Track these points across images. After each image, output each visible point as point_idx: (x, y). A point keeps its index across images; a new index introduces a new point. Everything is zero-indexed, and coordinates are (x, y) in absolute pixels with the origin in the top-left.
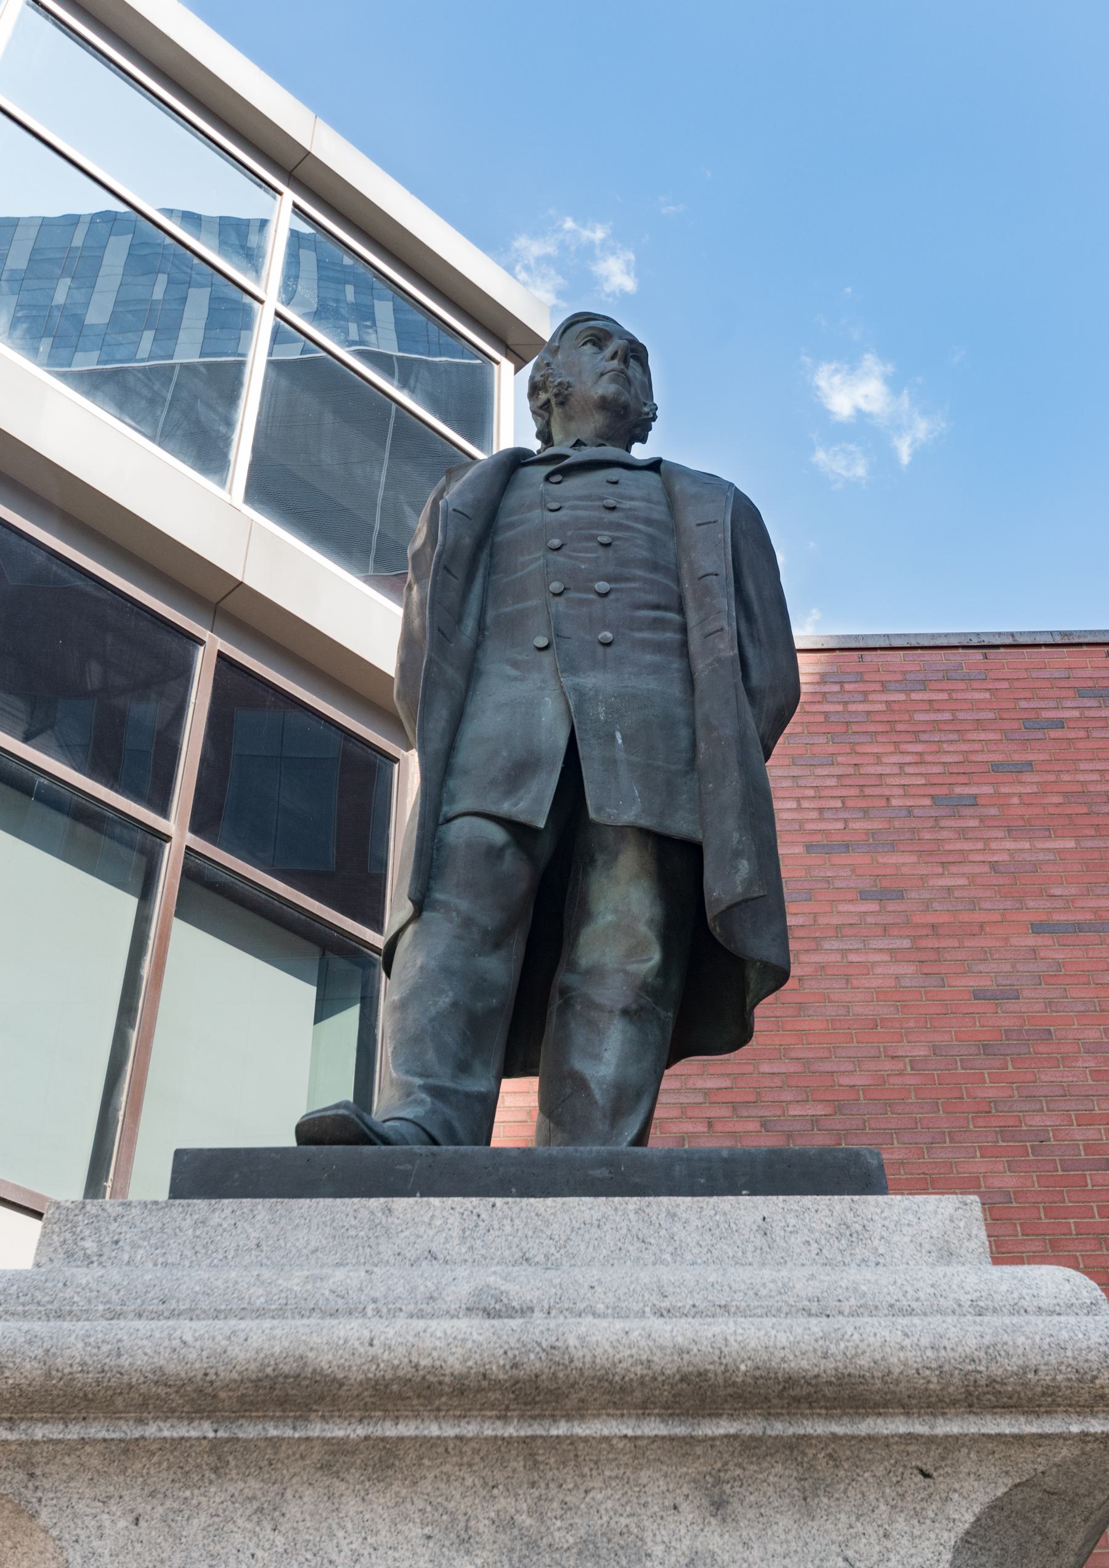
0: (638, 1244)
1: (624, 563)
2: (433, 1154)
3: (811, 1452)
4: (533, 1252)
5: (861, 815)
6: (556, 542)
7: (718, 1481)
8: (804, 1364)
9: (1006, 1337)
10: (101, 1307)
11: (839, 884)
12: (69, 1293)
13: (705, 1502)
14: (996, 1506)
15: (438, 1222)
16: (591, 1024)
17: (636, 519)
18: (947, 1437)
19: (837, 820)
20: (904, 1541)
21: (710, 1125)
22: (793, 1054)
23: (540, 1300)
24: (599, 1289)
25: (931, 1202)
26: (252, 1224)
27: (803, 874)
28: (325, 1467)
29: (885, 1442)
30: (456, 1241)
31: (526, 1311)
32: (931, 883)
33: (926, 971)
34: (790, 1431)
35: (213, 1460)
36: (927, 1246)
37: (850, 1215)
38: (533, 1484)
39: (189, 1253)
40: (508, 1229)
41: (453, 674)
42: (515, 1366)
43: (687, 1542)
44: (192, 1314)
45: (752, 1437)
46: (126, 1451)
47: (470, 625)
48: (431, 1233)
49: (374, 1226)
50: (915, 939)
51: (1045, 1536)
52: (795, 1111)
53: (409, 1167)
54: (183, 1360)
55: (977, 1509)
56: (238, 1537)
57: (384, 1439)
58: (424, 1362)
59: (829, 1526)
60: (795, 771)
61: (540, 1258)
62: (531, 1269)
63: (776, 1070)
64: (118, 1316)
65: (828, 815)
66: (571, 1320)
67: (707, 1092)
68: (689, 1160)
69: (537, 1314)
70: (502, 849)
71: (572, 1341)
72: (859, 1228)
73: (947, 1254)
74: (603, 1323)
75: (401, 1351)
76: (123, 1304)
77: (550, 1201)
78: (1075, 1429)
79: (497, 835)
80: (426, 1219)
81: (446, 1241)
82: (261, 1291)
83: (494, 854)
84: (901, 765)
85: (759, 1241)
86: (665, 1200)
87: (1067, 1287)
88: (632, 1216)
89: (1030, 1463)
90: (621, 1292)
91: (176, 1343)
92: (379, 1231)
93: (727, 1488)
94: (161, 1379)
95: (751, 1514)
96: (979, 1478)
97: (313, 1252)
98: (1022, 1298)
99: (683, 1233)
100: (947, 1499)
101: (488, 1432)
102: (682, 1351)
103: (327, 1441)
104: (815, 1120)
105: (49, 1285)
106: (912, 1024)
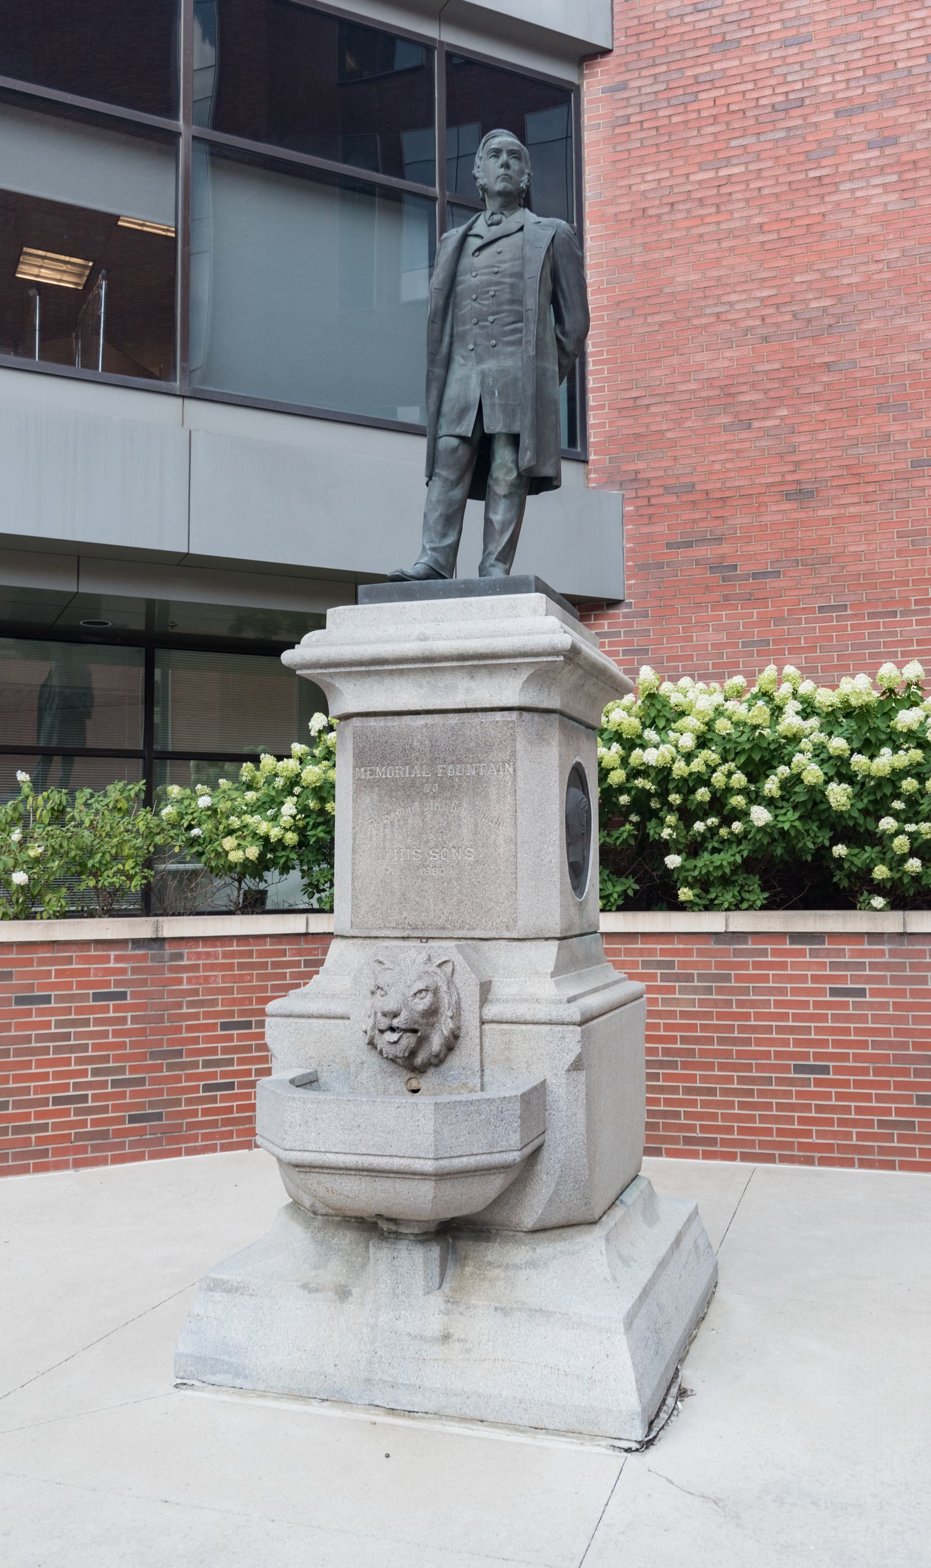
1: (500, 304)
5: (875, 80)
6: (474, 296)
11: (855, 139)
16: (495, 500)
17: (505, 276)
19: (859, 87)
21: (763, 320)
22: (816, 267)
27: (831, 135)
32: (917, 128)
33: (905, 197)
41: (439, 371)
47: (446, 339)
50: (901, 173)
52: (814, 305)
60: (833, 51)
63: (804, 280)
65: (852, 84)
67: (763, 299)
70: (457, 447)
73: (535, 611)
79: (455, 442)
83: (455, 450)
84: (908, 32)
89: (537, 667)
104: (825, 309)
106: (891, 237)
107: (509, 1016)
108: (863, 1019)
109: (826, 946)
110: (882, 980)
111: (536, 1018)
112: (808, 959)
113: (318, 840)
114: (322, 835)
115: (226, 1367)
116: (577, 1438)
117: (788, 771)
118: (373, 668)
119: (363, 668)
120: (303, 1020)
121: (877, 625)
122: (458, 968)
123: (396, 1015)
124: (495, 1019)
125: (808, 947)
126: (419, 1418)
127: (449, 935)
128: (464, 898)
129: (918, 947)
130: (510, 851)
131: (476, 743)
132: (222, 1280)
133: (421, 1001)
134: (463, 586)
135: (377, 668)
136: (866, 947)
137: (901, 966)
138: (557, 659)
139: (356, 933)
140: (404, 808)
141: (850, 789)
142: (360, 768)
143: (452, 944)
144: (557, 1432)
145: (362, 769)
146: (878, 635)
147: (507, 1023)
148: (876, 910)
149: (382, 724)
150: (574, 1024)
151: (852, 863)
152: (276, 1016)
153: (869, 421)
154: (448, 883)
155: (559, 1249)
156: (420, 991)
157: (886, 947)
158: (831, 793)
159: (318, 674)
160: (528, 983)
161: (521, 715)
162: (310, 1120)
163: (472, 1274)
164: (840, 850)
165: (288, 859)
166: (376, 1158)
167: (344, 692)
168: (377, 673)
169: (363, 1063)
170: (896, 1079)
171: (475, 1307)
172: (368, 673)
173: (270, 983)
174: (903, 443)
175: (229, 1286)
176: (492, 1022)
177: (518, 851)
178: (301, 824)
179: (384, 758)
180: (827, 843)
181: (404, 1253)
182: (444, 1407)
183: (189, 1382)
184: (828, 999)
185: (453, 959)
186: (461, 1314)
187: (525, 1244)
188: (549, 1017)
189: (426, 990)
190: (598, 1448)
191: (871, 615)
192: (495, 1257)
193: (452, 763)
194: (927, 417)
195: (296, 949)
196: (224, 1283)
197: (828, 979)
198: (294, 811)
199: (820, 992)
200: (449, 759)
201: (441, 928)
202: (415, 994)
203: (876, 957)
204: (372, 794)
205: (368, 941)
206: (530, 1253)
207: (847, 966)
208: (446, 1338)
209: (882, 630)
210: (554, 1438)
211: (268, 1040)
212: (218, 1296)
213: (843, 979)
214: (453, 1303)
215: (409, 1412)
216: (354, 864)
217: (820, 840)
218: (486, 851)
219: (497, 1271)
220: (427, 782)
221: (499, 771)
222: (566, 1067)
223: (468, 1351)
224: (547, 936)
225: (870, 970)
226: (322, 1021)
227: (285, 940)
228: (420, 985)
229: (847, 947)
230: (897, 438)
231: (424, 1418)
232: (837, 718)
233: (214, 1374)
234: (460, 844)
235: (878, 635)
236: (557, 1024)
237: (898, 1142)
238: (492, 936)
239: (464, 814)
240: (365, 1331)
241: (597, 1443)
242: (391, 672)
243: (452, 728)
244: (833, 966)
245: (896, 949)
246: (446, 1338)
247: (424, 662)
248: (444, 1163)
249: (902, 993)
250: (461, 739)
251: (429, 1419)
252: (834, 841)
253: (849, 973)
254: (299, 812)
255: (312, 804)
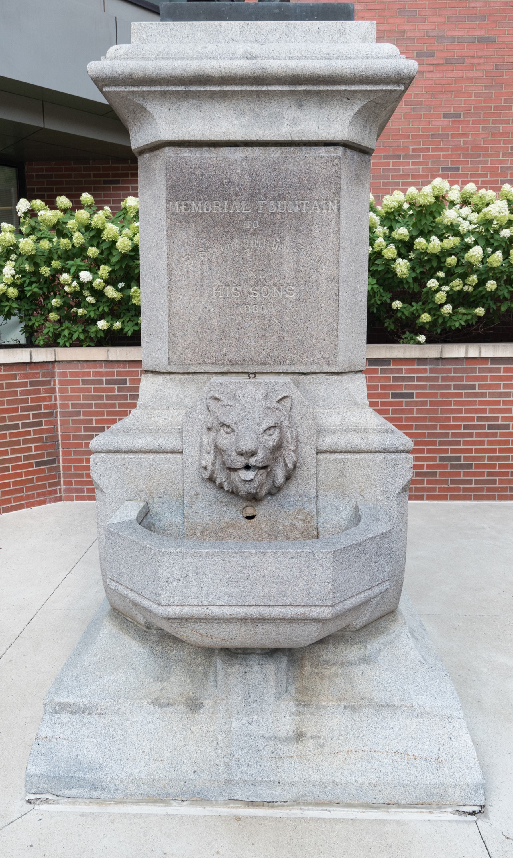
0: (285, 36)
2: (231, 5)
3: (322, 94)
4: (258, 38)
7: (301, 101)
8: (322, 73)
9: (371, 66)
10: (153, 56)
12: (144, 52)
13: (297, 105)
14: (364, 107)
15: (234, 29)
18: (354, 90)
20: (342, 115)
23: (260, 54)
24: (275, 51)
25: (363, 22)
26: (185, 30)
28: (211, 97)
29: (340, 91)
30: (238, 35)
31: (256, 57)
34: (318, 89)
35: (185, 95)
36: (360, 37)
37: (341, 27)
38: (258, 101)
39: (170, 39)
40: (252, 31)
42: (254, 73)
43: (293, 115)
44: (176, 58)
45: (309, 90)
46: (165, 93)
48: (232, 33)
49: (217, 30)
51: (375, 113)
53: (224, 9)
54: (176, 71)
55: (359, 107)
56: (192, 113)
57: (224, 91)
58: (233, 72)
59: (325, 111)
61: (260, 40)
62: (258, 44)
64: (158, 58)
66: (268, 60)
68: (301, 7)
69: (260, 58)
71: (268, 67)
72: (343, 31)
73: (364, 39)
74: (275, 61)
75: (227, 69)
76: (158, 55)
77: (263, 22)
78: (384, 88)
80: (230, 28)
81: (236, 35)
82: (191, 51)
85: (317, 35)
86: (293, 22)
87: (391, 50)
88: (284, 27)
90: (280, 52)
91: (174, 67)
92: (218, 32)
93: (302, 102)
94: (172, 77)
95: (308, 108)
96: (360, 100)
97: (202, 38)
98: (379, 53)
99: (297, 33)
100: (353, 105)
101: (248, 89)
102: (294, 69)
103: (211, 91)
105: (139, 49)
107: (344, 446)
108: (411, 411)
109: (391, 367)
110: (424, 387)
111: (371, 448)
112: (379, 375)
113: (34, 294)
114: (36, 290)
115: (82, 782)
116: (426, 808)
117: (372, 249)
118: (193, 88)
119: (182, 88)
120: (131, 456)
121: (388, 164)
122: (296, 402)
123: (253, 454)
124: (330, 449)
125: (379, 368)
126: (278, 806)
127: (270, 370)
128: (285, 334)
129: (447, 367)
130: (332, 289)
131: (299, 179)
132: (67, 703)
133: (271, 437)
134: (277, 11)
135: (199, 88)
136: (416, 367)
137: (436, 379)
138: (398, 88)
139: (174, 369)
140: (223, 245)
141: (408, 264)
142: (174, 202)
143: (287, 379)
144: (409, 806)
145: (177, 204)
146: (389, 170)
147: (341, 452)
148: (419, 343)
149: (198, 155)
150: (406, 452)
151: (403, 313)
152: (101, 452)
153: (392, 21)
154: (269, 320)
155: (382, 641)
156: (269, 428)
157: (428, 367)
158: (398, 266)
159: (129, 92)
160: (349, 414)
161: (345, 151)
162: (190, 574)
163: (311, 674)
164: (397, 304)
165: (11, 307)
166: (266, 608)
167: (156, 117)
168: (197, 95)
169: (197, 494)
170: (428, 447)
171: (325, 707)
172: (187, 95)
173: (6, 399)
174: (412, 39)
175: (76, 708)
176: (327, 452)
177: (340, 289)
178: (19, 282)
179: (200, 191)
180: (388, 301)
181: (256, 668)
182: (302, 796)
183: (44, 797)
184: (390, 400)
185: (291, 395)
186: (312, 714)
187: (356, 643)
188: (383, 447)
189: (274, 427)
190: (445, 814)
191: (386, 157)
192: (330, 656)
193: (273, 199)
194: (428, 22)
195: (23, 374)
196: (69, 705)
197: (391, 387)
198: (13, 272)
199: (386, 396)
200: (270, 195)
201: (261, 364)
202: (265, 431)
203: (422, 373)
204: (188, 230)
205: (186, 377)
206: (363, 651)
207: (403, 379)
208: (299, 736)
209: (391, 167)
210: (405, 810)
211: (94, 476)
212: (65, 717)
213: (400, 387)
214: (304, 706)
215: (268, 802)
216: (169, 301)
217: (384, 299)
218: (307, 289)
219: (334, 668)
220: (247, 219)
221: (322, 209)
222: (398, 491)
223: (322, 746)
224: (357, 370)
225: (417, 381)
226: (151, 456)
227: (14, 367)
228: (269, 422)
229: (404, 367)
230: (408, 35)
231: (283, 806)
232: (395, 217)
233: (70, 789)
234: (281, 282)
235: (389, 170)
236: (390, 452)
237: (427, 484)
238: (313, 370)
239: (285, 252)
240: (219, 737)
241: (443, 810)
242: (213, 95)
243: (274, 162)
244: (395, 379)
245: (433, 368)
246: (299, 736)
247: (252, 85)
248: (339, 608)
249: (435, 395)
250: (283, 174)
251: (288, 806)
252: (393, 299)
253: (404, 384)
254: (17, 273)
255: (27, 267)
